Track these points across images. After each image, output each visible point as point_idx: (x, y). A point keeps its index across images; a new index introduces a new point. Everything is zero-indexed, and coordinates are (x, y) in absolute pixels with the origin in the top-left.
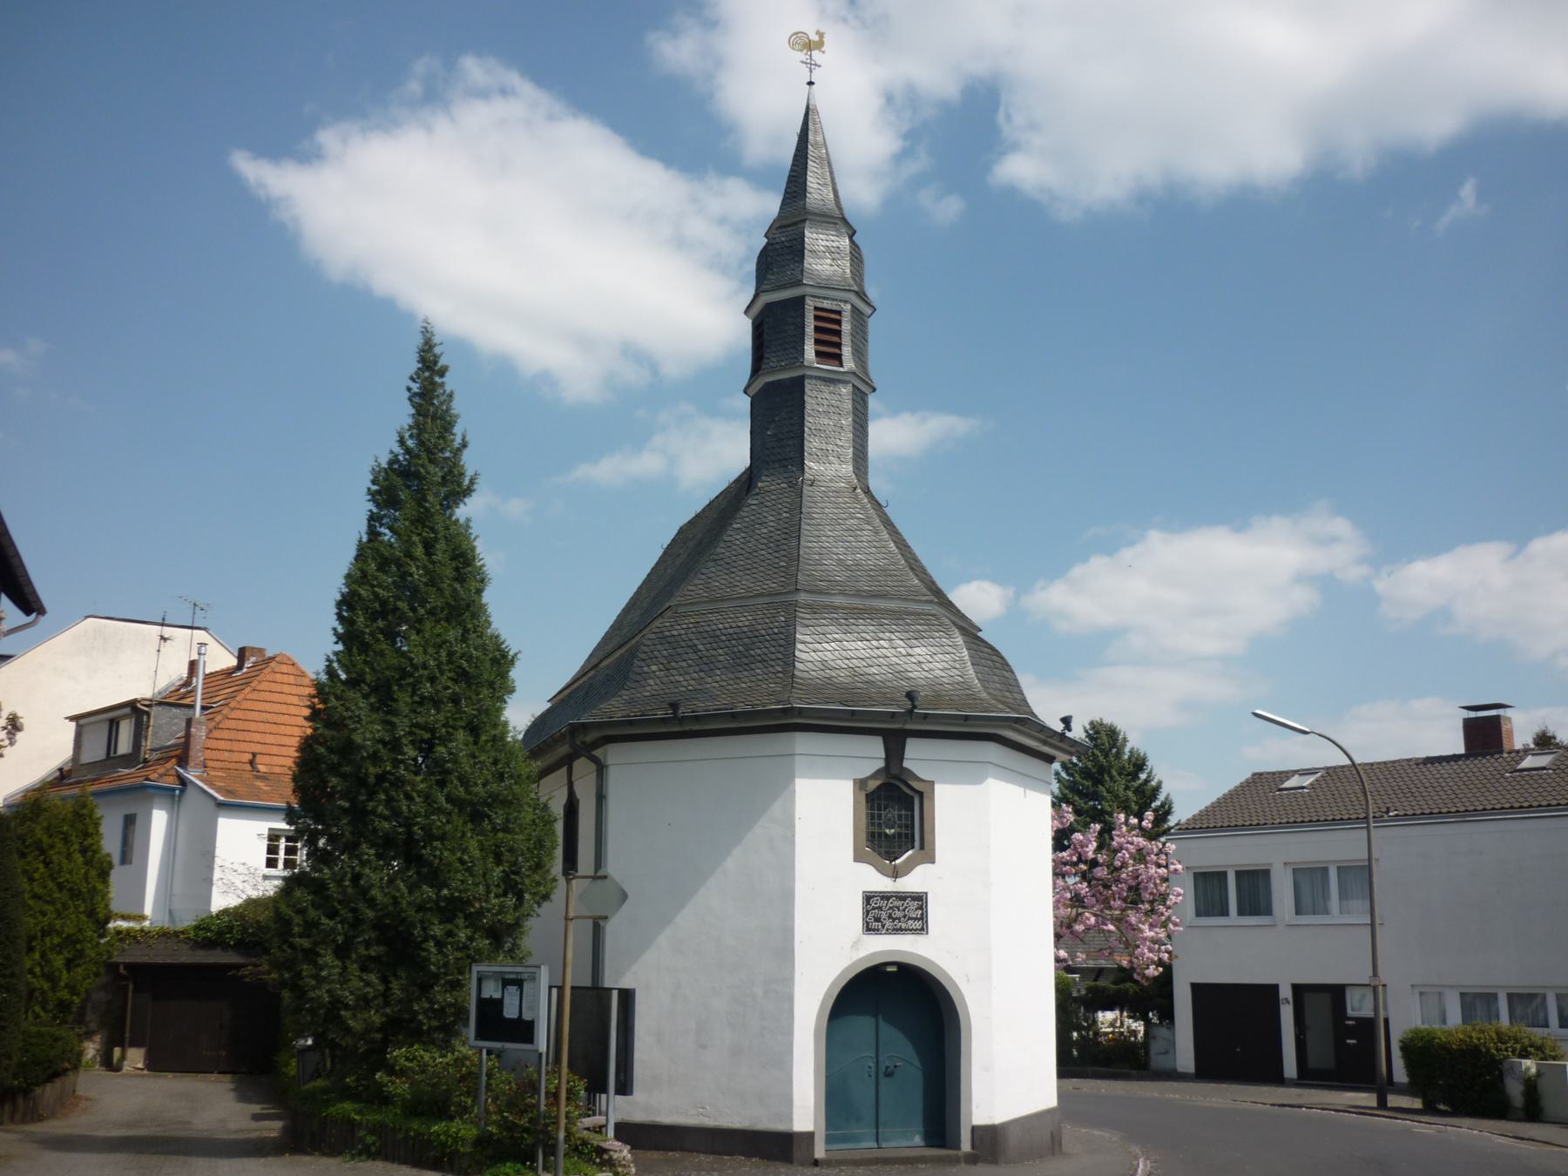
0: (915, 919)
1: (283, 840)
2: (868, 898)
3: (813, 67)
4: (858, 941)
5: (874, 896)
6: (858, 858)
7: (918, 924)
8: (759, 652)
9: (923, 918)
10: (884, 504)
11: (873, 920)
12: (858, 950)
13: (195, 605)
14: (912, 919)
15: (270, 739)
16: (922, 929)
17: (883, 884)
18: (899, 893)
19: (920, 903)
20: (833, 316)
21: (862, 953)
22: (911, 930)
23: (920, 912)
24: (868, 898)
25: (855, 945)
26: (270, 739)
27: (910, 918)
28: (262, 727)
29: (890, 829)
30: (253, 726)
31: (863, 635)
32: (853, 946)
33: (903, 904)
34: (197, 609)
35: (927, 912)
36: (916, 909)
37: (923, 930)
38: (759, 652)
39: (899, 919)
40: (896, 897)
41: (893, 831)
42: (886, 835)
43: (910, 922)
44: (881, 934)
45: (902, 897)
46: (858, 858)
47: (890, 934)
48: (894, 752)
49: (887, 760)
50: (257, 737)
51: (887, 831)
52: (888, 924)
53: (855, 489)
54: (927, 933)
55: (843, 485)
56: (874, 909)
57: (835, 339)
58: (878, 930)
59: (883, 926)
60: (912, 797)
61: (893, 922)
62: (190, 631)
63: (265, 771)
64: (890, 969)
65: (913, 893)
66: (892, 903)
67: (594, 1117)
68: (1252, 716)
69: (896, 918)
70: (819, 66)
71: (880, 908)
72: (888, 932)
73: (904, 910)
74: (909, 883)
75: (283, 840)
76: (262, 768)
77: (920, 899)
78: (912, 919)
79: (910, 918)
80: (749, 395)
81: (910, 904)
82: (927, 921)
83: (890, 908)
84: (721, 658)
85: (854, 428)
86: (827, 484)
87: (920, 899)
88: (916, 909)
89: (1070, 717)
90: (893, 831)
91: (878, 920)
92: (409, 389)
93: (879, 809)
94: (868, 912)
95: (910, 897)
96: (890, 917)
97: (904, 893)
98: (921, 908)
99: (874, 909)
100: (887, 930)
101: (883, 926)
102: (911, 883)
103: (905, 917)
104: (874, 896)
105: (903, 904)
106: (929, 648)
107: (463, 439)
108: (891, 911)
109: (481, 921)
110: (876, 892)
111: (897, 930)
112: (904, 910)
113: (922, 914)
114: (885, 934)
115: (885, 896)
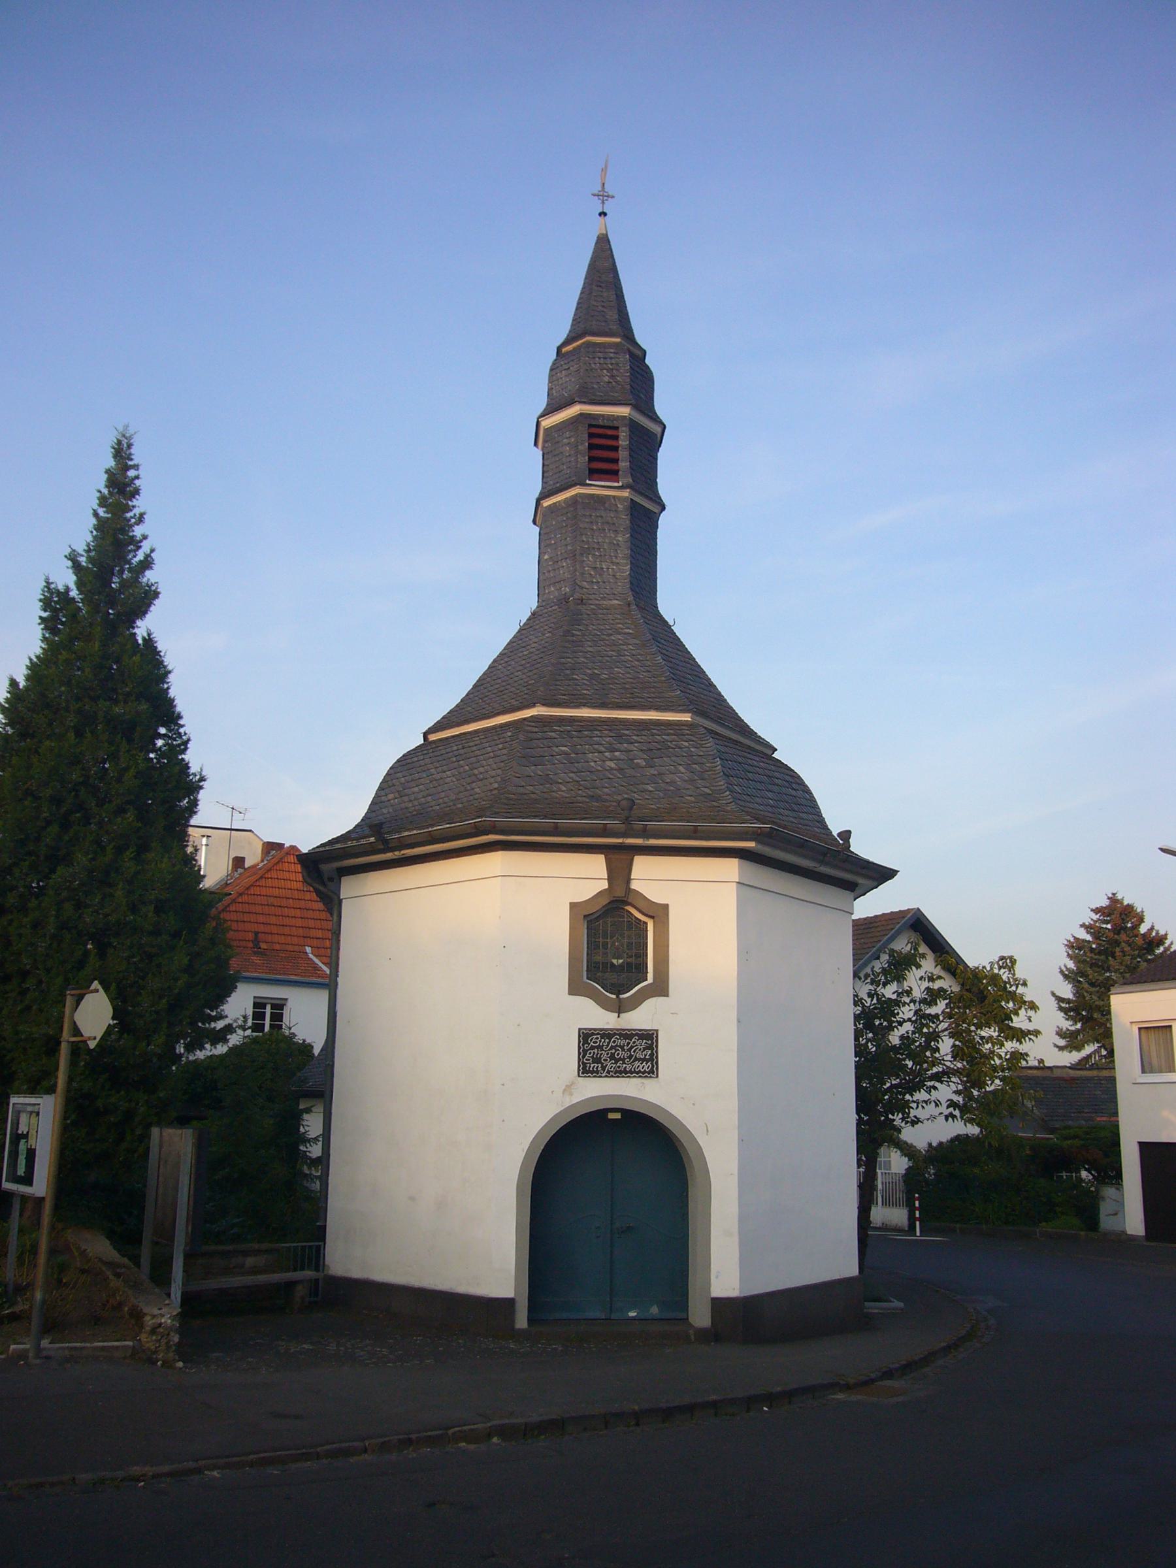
0: (643, 1060)
1: (268, 1007)
2: (585, 1036)
3: (605, 198)
4: (571, 1085)
5: (593, 1034)
6: (575, 988)
7: (646, 1066)
8: (481, 769)
9: (653, 1059)
10: (671, 623)
11: (591, 1061)
12: (571, 1094)
13: (233, 808)
14: (639, 1060)
15: (273, 920)
16: (652, 1072)
17: (603, 1019)
18: (624, 1030)
19: (650, 1042)
20: (610, 432)
21: (576, 1099)
22: (637, 1073)
23: (650, 1052)
24: (585, 1036)
25: (568, 1089)
26: (273, 920)
27: (636, 1059)
28: (266, 910)
29: (618, 958)
30: (258, 909)
31: (596, 746)
32: (565, 1090)
33: (628, 1044)
34: (236, 814)
35: (657, 1052)
36: (644, 1049)
37: (652, 1072)
38: (481, 769)
39: (624, 1060)
40: (620, 1035)
41: (621, 961)
42: (612, 964)
43: (637, 1063)
44: (600, 1077)
45: (627, 1035)
46: (575, 988)
47: (612, 1076)
48: (619, 873)
49: (610, 879)
50: (261, 919)
51: (615, 961)
52: (610, 1065)
53: (629, 605)
54: (657, 1076)
55: (616, 602)
56: (593, 1048)
57: (611, 455)
58: (597, 1072)
59: (603, 1068)
60: (646, 923)
61: (616, 1063)
62: (229, 831)
63: (266, 948)
64: (611, 1116)
65: (640, 1030)
66: (614, 1042)
67: (294, 1273)
68: (1159, 851)
69: (620, 1059)
70: (613, 197)
71: (600, 1047)
72: (609, 1075)
73: (629, 1050)
74: (637, 1019)
75: (268, 1007)
76: (263, 946)
77: (649, 1038)
78: (639, 1060)
79: (636, 1059)
80: (537, 526)
81: (637, 1043)
82: (657, 1063)
83: (612, 1048)
84: (448, 780)
85: (632, 543)
86: (597, 602)
87: (649, 1038)
88: (644, 1049)
89: (849, 832)
90: (621, 961)
91: (597, 1060)
92: (96, 514)
93: (605, 936)
94: (585, 1052)
95: (637, 1034)
96: (612, 1057)
97: (629, 1030)
98: (650, 1047)
99: (593, 1048)
100: (608, 1072)
101: (603, 1068)
102: (638, 1019)
103: (630, 1057)
104: (593, 1034)
105: (628, 1044)
106: (674, 758)
107: (148, 556)
108: (613, 1051)
109: (981, 1138)
110: (595, 1030)
111: (621, 1072)
112: (629, 1050)
113: (652, 1055)
114: (606, 1076)
115: (606, 1034)
